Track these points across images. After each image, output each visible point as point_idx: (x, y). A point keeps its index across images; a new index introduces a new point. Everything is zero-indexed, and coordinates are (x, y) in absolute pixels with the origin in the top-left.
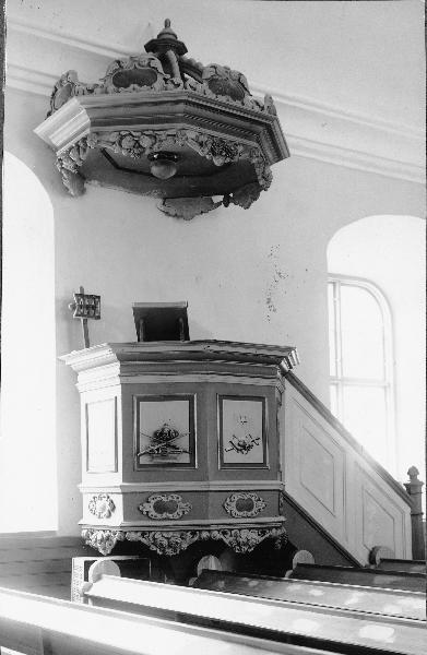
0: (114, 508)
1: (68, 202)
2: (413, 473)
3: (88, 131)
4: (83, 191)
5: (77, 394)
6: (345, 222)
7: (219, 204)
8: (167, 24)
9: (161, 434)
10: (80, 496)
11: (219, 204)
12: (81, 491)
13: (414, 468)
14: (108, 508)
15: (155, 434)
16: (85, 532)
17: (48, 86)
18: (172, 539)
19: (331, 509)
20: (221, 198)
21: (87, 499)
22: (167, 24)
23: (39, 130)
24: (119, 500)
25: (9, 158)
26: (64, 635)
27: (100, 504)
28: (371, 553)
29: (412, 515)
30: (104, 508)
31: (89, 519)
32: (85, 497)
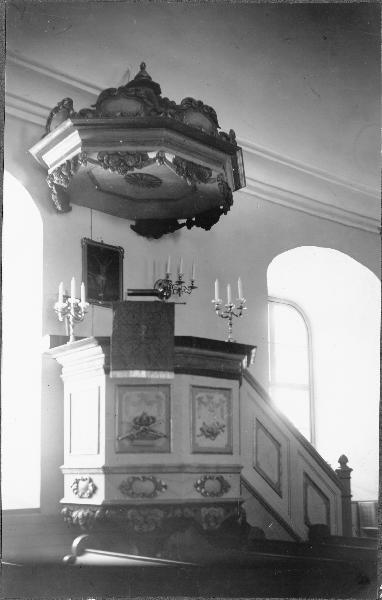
0: (95, 489)
1: (55, 217)
2: (343, 460)
3: (79, 150)
4: (67, 209)
5: (61, 384)
6: (275, 255)
7: (183, 225)
8: (143, 67)
9: (141, 419)
10: (61, 478)
11: (183, 225)
12: (64, 472)
13: (344, 456)
14: (91, 488)
15: (135, 419)
16: (65, 510)
17: (44, 117)
18: (150, 517)
19: (310, 489)
20: (184, 221)
21: (69, 481)
22: (143, 67)
23: (34, 151)
24: (100, 481)
25: (8, 177)
26: (35, 200)
27: (82, 485)
28: (306, 523)
29: (342, 497)
30: (87, 488)
31: (70, 497)
32: (66, 477)
